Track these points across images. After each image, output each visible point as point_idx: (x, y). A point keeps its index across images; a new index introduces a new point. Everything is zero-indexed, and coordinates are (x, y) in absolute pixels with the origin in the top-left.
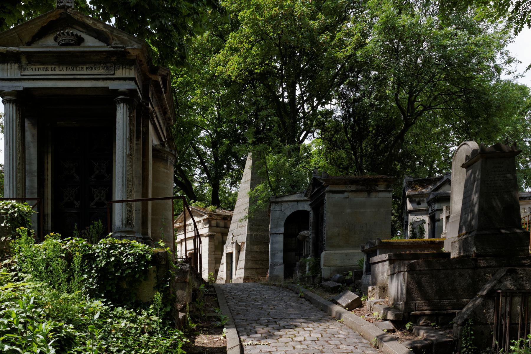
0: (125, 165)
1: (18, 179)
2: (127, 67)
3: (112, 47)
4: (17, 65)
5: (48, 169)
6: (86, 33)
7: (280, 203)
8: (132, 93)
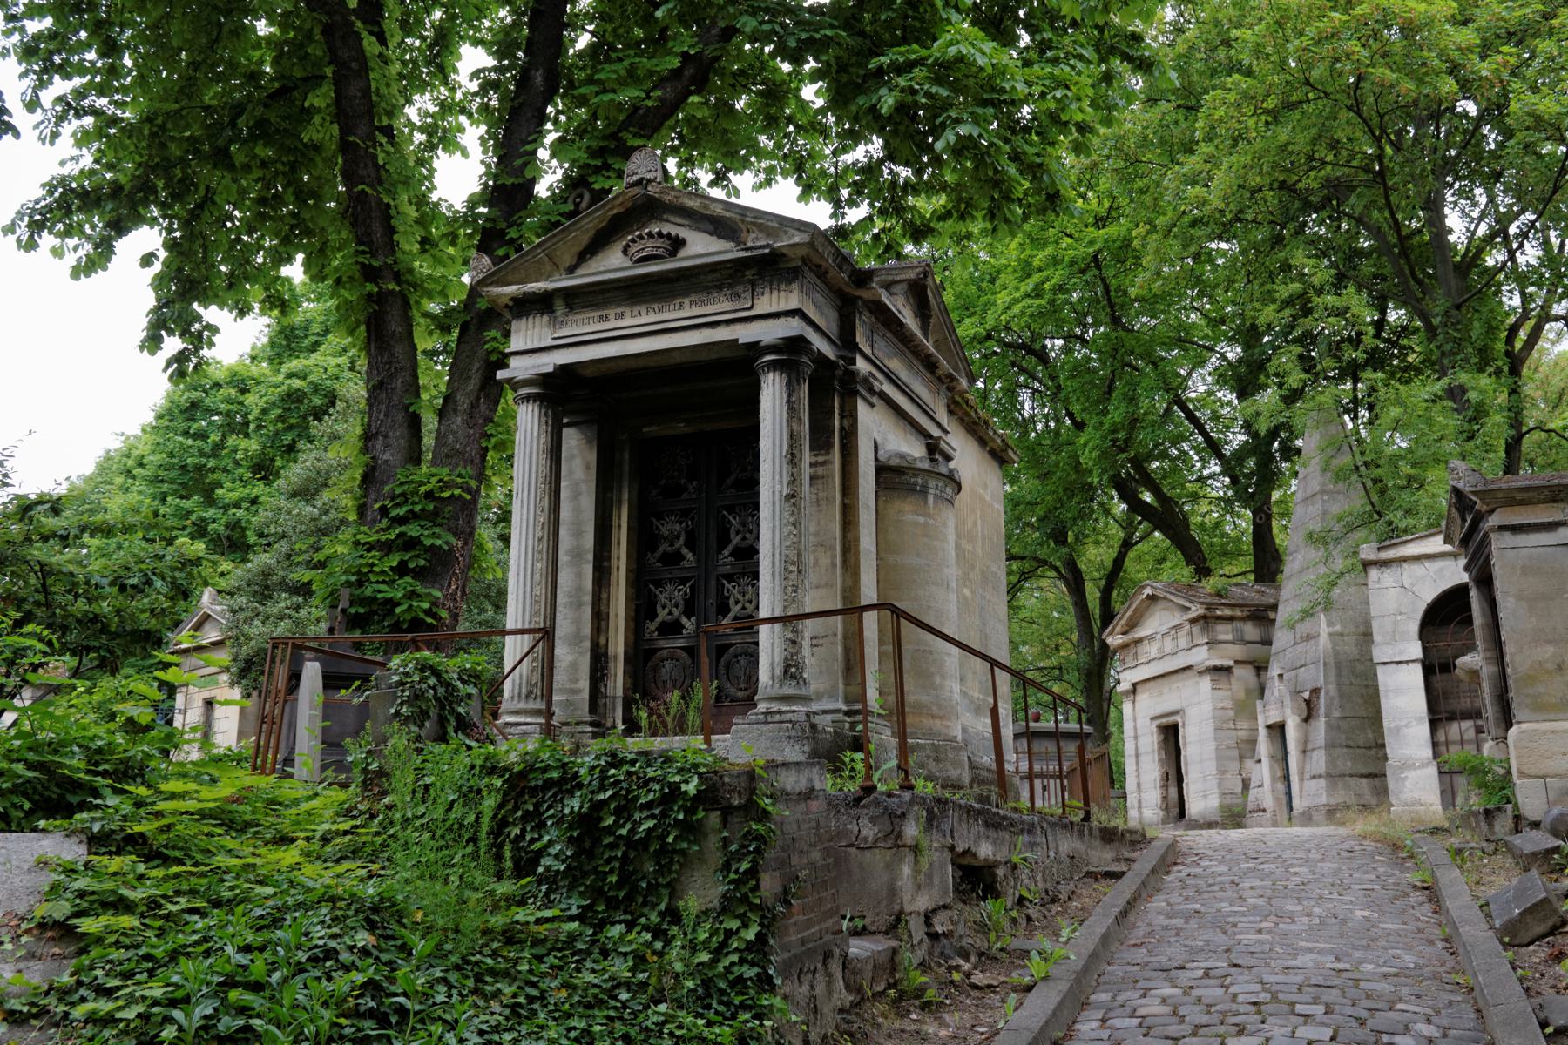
1: (537, 576)
2: (783, 287)
4: (546, 318)
8: (795, 345)
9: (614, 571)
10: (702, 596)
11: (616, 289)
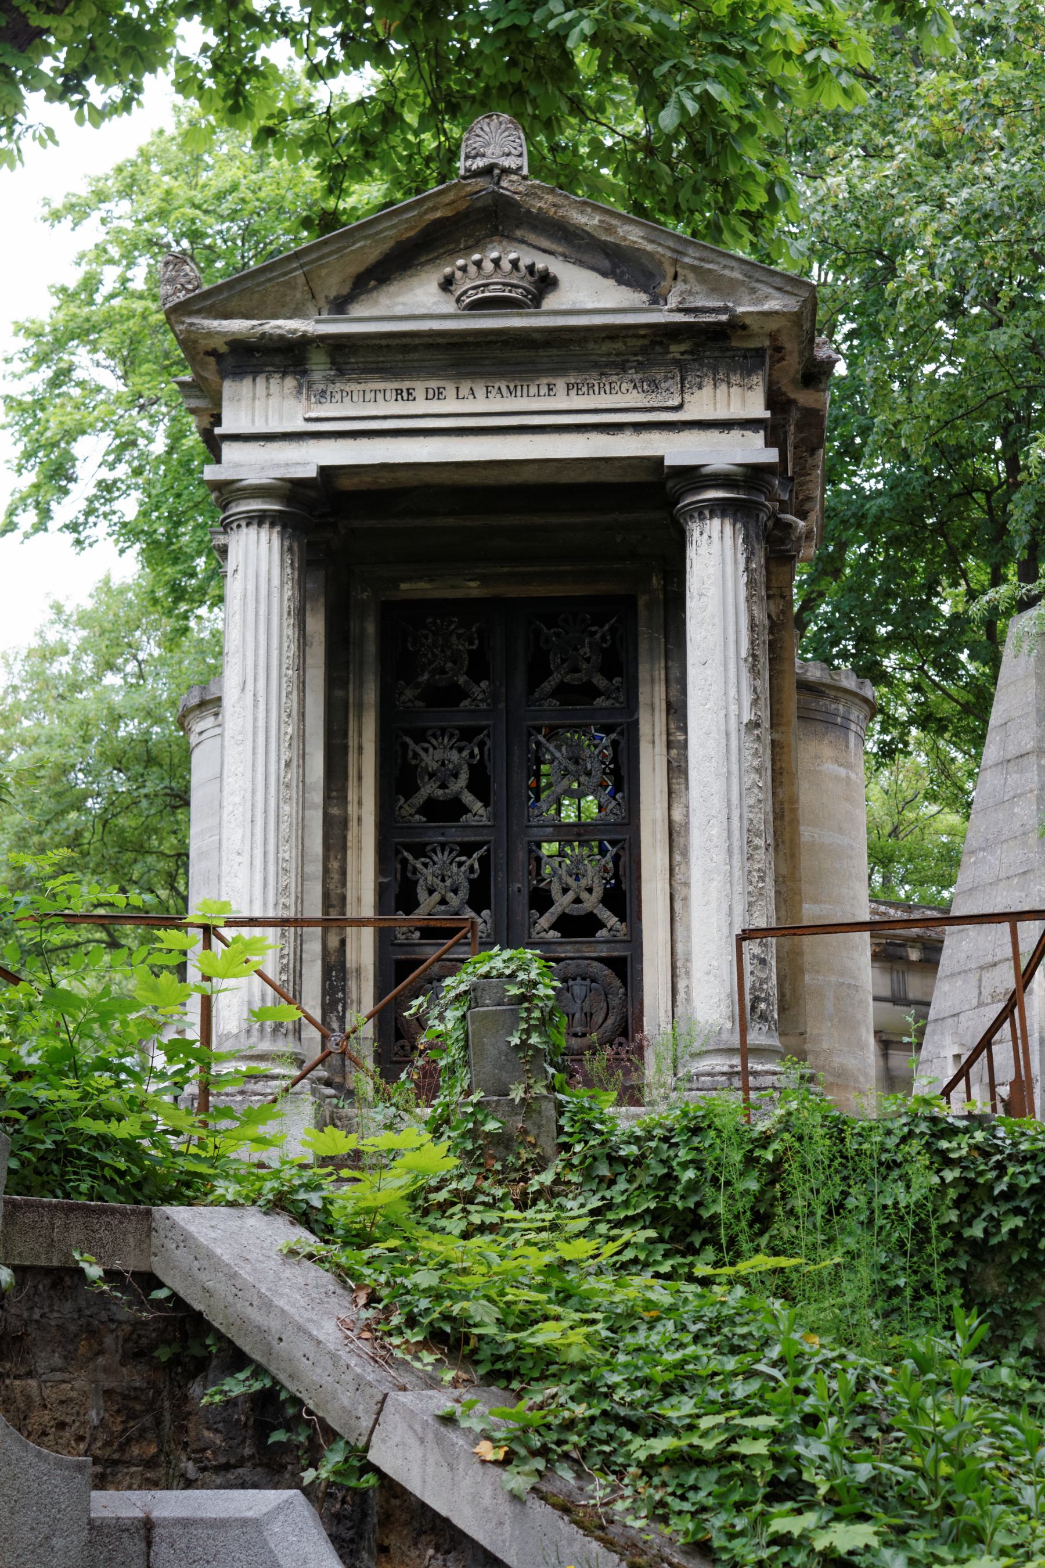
0: (735, 768)
1: (284, 826)
2: (735, 379)
3: (671, 311)
5: (360, 778)
6: (566, 257)
7: (73, 957)
9: (353, 824)
10: (502, 875)
11: (430, 346)
